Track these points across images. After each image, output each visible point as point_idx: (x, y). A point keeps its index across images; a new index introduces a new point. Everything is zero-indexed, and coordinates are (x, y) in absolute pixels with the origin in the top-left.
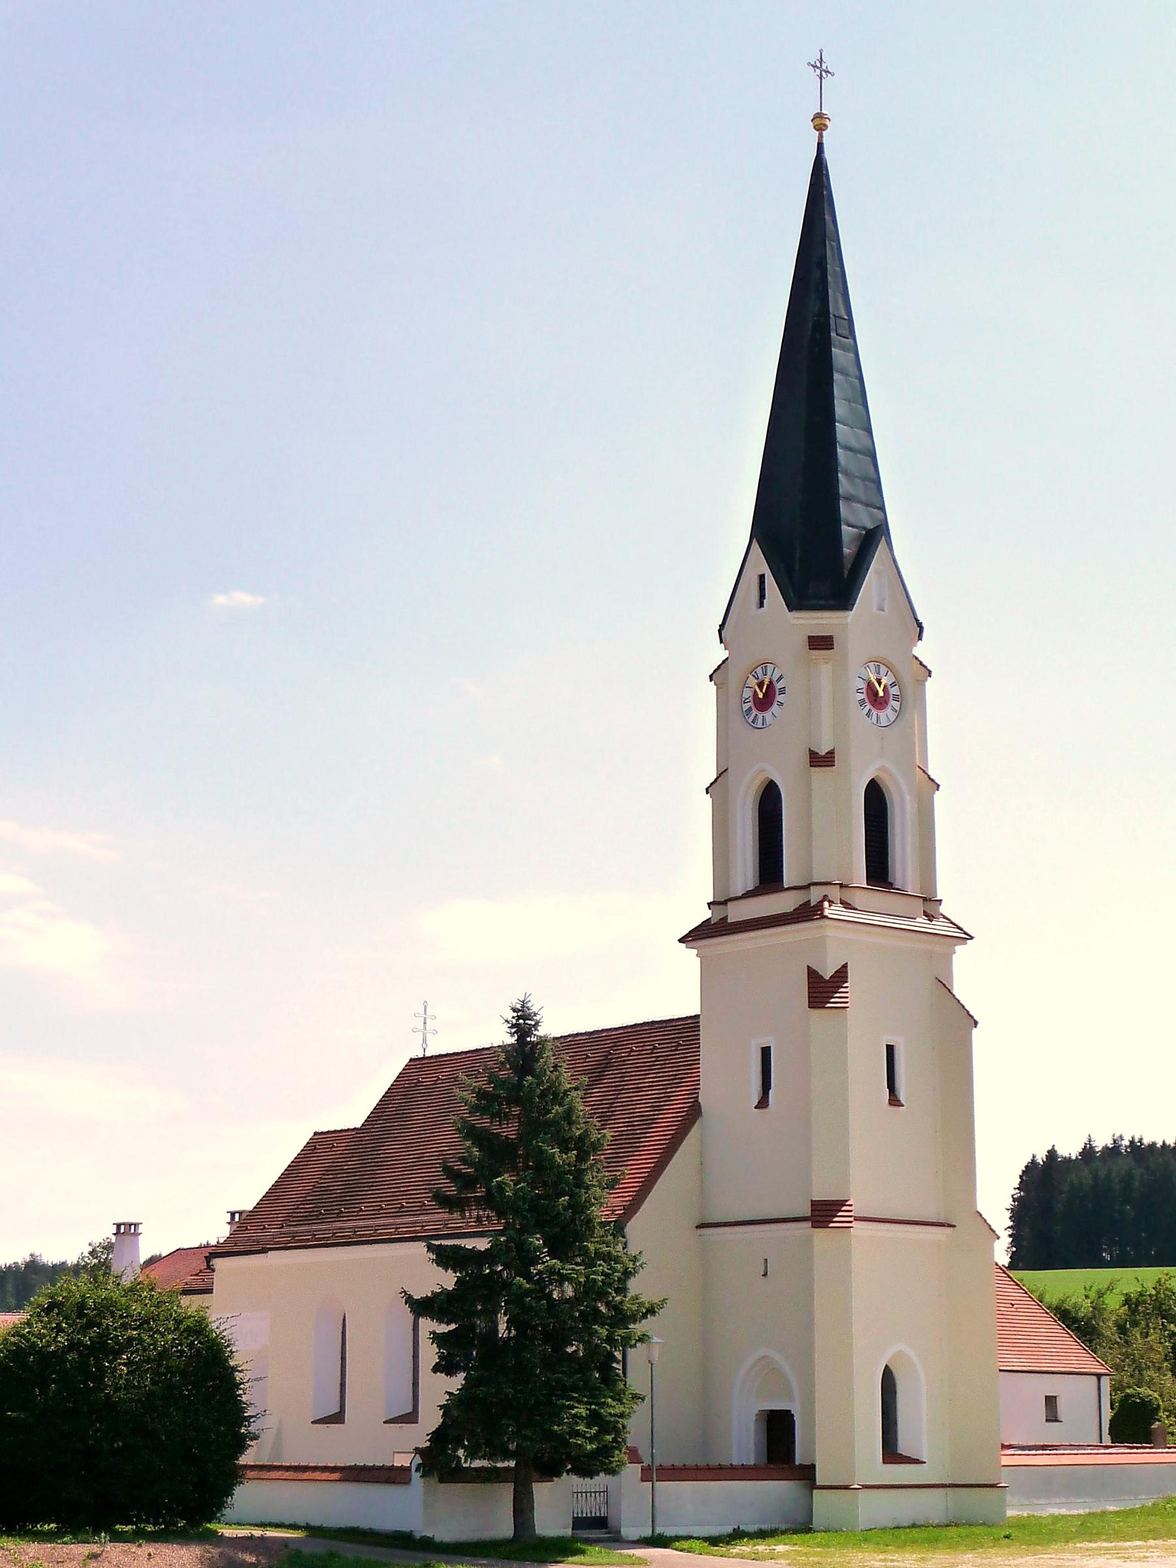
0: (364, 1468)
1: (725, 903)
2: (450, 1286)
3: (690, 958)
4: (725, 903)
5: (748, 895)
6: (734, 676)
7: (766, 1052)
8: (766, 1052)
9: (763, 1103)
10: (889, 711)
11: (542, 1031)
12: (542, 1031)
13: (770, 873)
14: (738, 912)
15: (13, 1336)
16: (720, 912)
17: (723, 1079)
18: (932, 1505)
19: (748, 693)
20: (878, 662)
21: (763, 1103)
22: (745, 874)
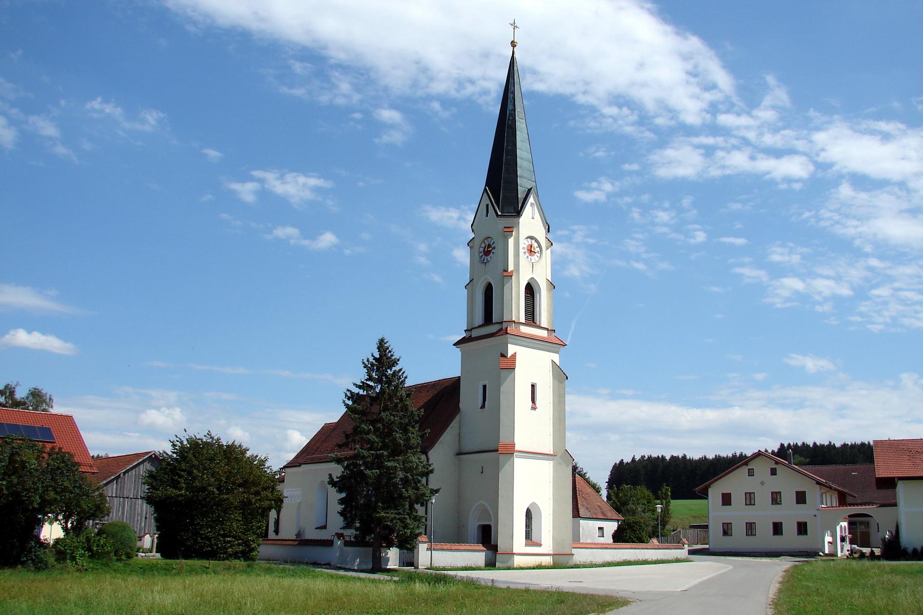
0: (318, 541)
1: (471, 330)
2: (274, 231)
3: (457, 352)
4: (471, 330)
5: (480, 326)
6: (477, 244)
7: (485, 387)
8: (485, 387)
9: (483, 406)
10: (535, 256)
11: (408, 383)
12: (408, 383)
13: (488, 318)
14: (475, 334)
15: (611, 104)
16: (469, 334)
17: (468, 399)
18: (548, 560)
19: (482, 249)
20: (531, 238)
21: (483, 406)
22: (479, 319)
